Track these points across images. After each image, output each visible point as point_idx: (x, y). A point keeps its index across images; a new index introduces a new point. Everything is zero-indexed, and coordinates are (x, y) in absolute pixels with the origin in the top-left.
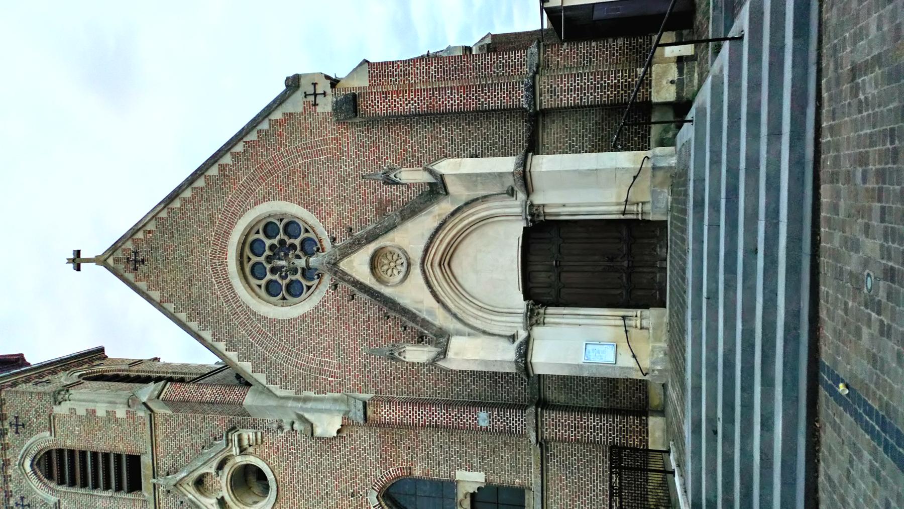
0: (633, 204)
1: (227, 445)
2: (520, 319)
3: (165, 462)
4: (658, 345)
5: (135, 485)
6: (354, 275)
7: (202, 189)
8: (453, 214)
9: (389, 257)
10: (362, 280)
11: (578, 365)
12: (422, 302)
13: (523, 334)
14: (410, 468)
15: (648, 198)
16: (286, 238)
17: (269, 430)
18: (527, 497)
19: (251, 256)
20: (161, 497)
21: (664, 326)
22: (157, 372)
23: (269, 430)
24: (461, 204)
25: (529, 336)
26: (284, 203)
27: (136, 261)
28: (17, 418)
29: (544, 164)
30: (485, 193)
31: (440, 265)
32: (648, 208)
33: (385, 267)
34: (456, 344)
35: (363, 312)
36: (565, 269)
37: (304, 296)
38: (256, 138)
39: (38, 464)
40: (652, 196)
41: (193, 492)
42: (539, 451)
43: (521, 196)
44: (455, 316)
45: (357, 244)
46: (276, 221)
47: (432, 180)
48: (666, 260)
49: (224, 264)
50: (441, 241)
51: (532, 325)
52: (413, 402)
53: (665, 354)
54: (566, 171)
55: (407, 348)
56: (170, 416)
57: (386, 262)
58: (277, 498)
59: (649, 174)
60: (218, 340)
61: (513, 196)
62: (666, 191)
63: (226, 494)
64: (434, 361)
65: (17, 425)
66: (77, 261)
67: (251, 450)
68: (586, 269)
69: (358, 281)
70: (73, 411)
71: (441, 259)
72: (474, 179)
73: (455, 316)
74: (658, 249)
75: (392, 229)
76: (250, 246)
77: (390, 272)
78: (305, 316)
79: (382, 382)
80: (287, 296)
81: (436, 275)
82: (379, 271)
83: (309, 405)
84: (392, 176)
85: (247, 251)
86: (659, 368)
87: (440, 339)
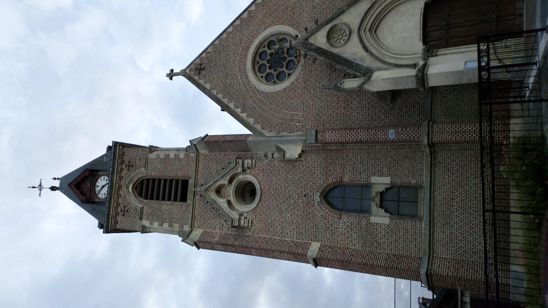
1: (236, 165)
3: (201, 181)
5: (184, 199)
6: (317, 44)
9: (339, 33)
10: (321, 47)
11: (460, 71)
12: (357, 54)
13: (421, 63)
14: (341, 177)
17: (259, 159)
18: (419, 195)
19: (259, 60)
20: (197, 202)
23: (259, 159)
27: (200, 69)
28: (129, 162)
31: (370, 31)
34: (376, 75)
35: (319, 83)
39: (136, 188)
41: (214, 195)
42: (429, 159)
44: (378, 59)
45: (319, 27)
48: (523, 9)
49: (245, 65)
50: (371, 16)
52: (346, 129)
56: (207, 155)
58: (260, 200)
63: (232, 198)
64: (361, 87)
65: (129, 166)
66: (171, 75)
67: (248, 171)
70: (158, 156)
73: (378, 59)
78: (286, 89)
79: (328, 123)
80: (277, 81)
82: (332, 41)
85: (258, 58)
87: (367, 73)
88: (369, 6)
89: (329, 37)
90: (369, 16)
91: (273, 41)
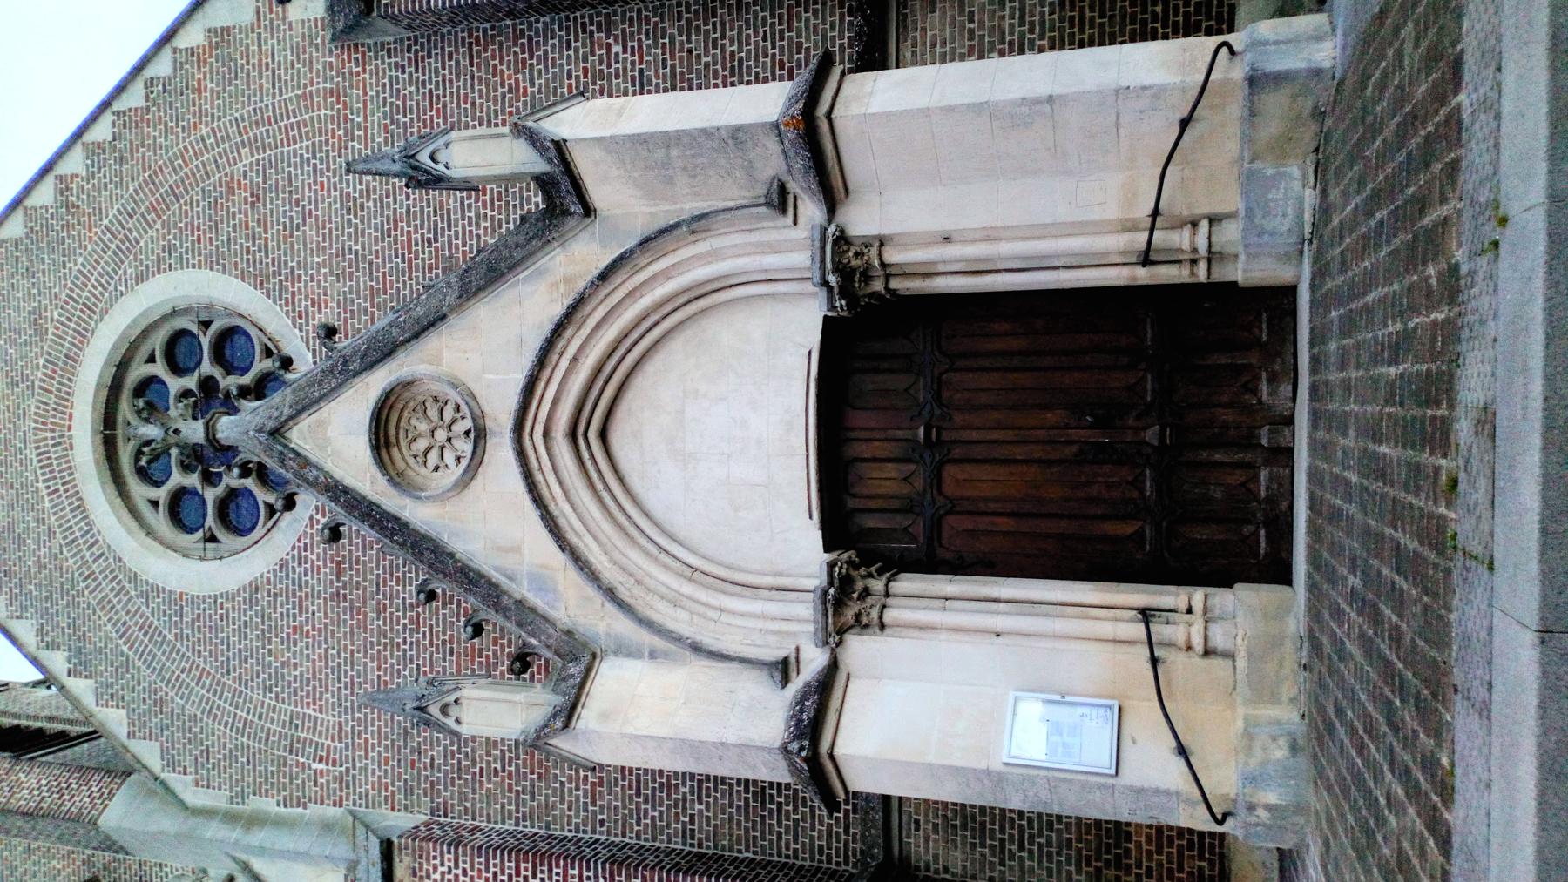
0: (1178, 224)
2: (805, 610)
4: (1269, 712)
6: (329, 465)
7: (17, 243)
8: (604, 276)
9: (433, 412)
11: (988, 772)
12: (516, 550)
13: (814, 659)
15: (1230, 199)
16: (217, 372)
21: (1289, 647)
22: (15, 716)
24: (631, 243)
25: (833, 666)
26: (205, 274)
29: (871, 100)
30: (702, 206)
31: (572, 435)
32: (1230, 234)
33: (421, 445)
34: (614, 683)
36: (958, 452)
37: (260, 530)
38: (142, 103)
40: (1245, 194)
43: (811, 210)
44: (610, 593)
45: (341, 373)
46: (194, 328)
47: (540, 166)
48: (1290, 421)
50: (575, 359)
51: (842, 631)
53: (1294, 748)
54: (950, 109)
55: (468, 692)
57: (423, 427)
59: (1236, 109)
60: (52, 646)
61: (784, 211)
62: (1295, 171)
64: (537, 742)
68: (1019, 452)
69: (337, 484)
71: (587, 423)
72: (660, 154)
73: (610, 593)
74: (1264, 388)
75: (432, 324)
76: (128, 392)
77: (433, 458)
81: (559, 464)
82: (402, 456)
83: (259, 837)
84: (424, 158)
86: (1272, 798)
87: (557, 662)
88: (558, 310)
89: (383, 433)
90: (564, 364)
91: (182, 334)
